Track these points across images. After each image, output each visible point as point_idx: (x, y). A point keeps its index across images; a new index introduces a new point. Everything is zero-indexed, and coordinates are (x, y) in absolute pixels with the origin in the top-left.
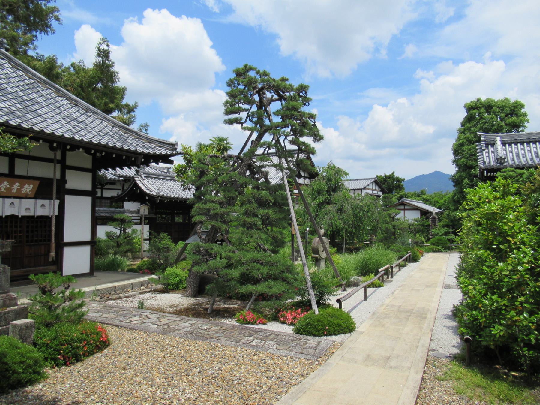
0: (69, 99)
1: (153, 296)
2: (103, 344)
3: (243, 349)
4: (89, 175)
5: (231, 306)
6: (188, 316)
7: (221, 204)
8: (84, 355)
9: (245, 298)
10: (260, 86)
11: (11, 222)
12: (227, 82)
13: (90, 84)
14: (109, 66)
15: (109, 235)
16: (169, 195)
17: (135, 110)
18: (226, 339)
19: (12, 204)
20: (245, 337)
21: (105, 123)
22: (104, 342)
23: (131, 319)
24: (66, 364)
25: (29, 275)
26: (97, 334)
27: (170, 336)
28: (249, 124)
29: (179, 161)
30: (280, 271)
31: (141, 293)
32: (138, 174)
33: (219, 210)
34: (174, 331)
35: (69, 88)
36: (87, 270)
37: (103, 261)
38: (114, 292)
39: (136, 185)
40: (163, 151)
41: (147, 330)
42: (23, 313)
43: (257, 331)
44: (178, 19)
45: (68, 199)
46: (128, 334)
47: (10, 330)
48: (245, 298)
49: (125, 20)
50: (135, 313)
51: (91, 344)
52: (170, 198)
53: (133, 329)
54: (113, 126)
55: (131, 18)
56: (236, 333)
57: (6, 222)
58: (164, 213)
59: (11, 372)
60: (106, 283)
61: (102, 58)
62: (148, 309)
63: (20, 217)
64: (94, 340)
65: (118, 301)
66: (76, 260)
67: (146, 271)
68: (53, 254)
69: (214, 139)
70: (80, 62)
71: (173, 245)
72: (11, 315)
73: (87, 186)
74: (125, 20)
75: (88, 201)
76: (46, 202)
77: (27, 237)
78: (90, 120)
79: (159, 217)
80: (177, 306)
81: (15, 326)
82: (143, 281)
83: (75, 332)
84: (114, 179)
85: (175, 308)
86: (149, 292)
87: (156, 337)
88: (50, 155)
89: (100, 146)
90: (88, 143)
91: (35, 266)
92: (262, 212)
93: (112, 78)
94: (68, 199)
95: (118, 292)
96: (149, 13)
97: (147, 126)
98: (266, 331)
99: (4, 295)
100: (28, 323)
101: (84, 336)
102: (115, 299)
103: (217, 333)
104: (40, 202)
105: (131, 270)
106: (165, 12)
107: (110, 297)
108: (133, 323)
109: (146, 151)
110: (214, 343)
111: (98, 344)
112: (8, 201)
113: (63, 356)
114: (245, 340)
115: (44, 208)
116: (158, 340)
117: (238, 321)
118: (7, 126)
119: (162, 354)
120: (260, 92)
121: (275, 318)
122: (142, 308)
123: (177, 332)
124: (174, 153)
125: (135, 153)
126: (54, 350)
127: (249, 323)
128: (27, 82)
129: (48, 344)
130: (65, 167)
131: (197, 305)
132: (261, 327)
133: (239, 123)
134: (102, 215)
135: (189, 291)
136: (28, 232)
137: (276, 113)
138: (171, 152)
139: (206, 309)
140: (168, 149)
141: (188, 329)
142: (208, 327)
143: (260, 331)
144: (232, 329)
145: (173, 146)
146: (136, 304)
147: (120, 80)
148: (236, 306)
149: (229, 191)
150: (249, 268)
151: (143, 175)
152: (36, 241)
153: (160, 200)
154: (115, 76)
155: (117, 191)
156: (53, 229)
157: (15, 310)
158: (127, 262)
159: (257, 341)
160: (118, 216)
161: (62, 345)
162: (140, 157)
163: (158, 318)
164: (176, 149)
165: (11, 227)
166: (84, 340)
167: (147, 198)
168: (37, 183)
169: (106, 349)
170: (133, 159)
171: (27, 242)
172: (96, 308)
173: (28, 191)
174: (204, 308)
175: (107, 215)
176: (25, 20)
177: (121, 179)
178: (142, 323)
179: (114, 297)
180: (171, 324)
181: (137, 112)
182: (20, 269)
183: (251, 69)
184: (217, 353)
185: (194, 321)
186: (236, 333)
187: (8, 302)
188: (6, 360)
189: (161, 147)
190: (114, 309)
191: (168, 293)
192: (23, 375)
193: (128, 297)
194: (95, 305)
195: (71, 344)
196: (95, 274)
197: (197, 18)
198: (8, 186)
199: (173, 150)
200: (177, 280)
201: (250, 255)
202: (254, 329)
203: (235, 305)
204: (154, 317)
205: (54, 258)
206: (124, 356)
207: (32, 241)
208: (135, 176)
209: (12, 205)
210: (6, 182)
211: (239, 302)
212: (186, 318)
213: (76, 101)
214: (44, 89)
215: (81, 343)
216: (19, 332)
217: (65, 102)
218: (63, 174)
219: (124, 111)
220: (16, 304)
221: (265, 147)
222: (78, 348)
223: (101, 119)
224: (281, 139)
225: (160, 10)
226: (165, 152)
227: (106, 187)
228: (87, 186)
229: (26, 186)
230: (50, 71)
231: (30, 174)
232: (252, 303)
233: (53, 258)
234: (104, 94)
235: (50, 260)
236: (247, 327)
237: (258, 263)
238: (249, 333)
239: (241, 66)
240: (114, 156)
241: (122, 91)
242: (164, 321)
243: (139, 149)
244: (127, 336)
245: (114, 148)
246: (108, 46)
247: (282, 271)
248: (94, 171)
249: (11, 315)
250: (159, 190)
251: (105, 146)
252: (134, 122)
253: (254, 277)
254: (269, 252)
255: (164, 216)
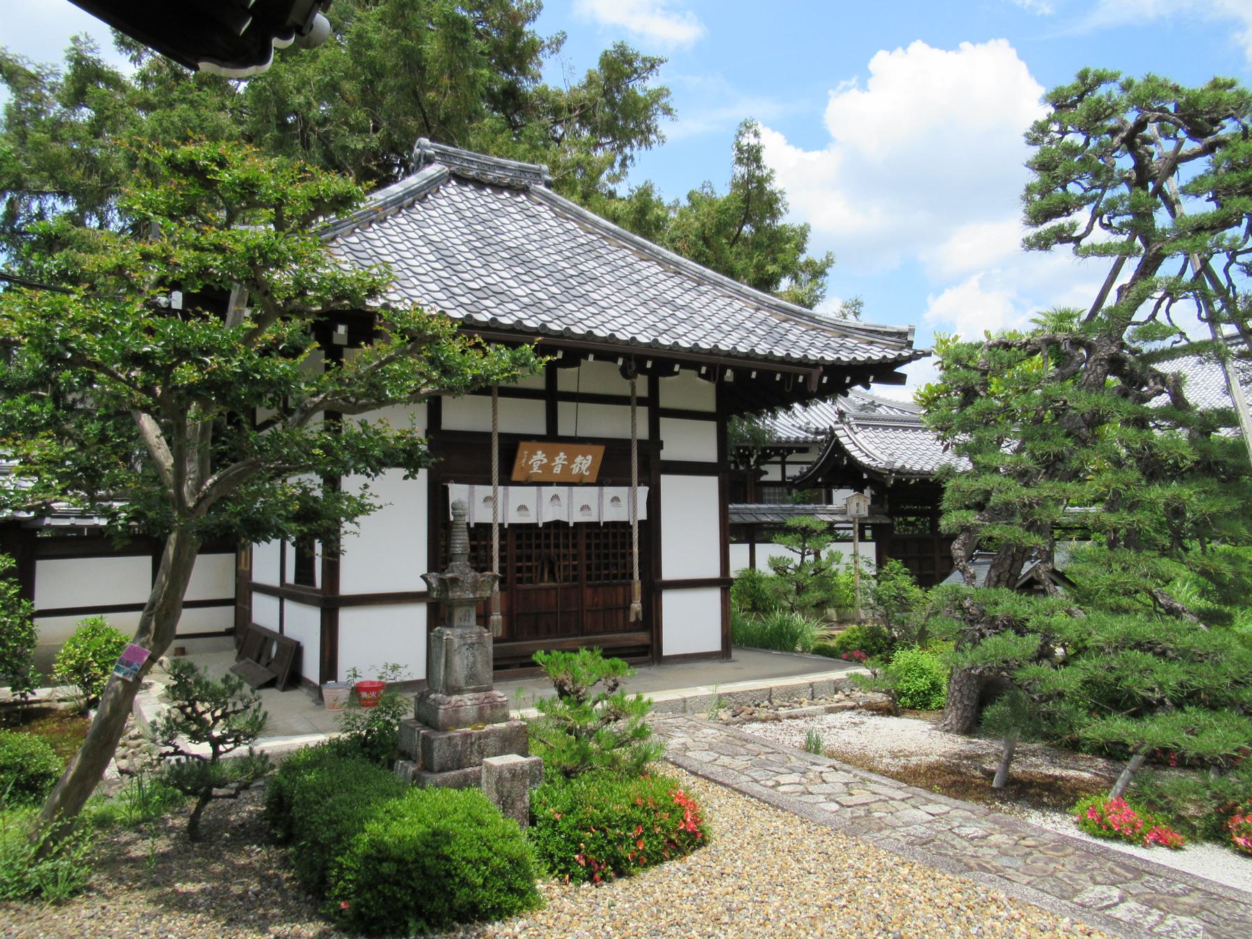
0: (664, 262)
1: (857, 720)
2: (689, 839)
3: (1078, 927)
4: (711, 427)
5: (1071, 773)
6: (929, 788)
7: (1023, 476)
8: (638, 862)
9: (1115, 752)
10: (1131, 117)
11: (557, 537)
12: (1027, 135)
13: (721, 228)
14: (761, 182)
15: (779, 567)
16: (917, 468)
17: (828, 270)
18: (1027, 879)
19: (555, 497)
20: (1096, 883)
21: (737, 305)
22: (688, 834)
23: (779, 778)
24: (591, 878)
25: (535, 652)
26: (673, 811)
27: (865, 842)
28: (1100, 236)
29: (923, 375)
30: (1228, 681)
31: (831, 711)
32: (842, 421)
33: (1016, 493)
34: (880, 830)
35: (679, 245)
36: (716, 646)
37: (756, 624)
38: (766, 703)
39: (839, 447)
40: (876, 353)
41: (811, 814)
42: (517, 740)
43: (1138, 870)
44: (951, 53)
45: (668, 482)
46: (762, 820)
47: (484, 776)
48: (1115, 752)
49: (831, 92)
50: (795, 762)
51: (656, 836)
52: (920, 473)
53: (778, 807)
54: (757, 309)
55: (843, 83)
56: (1066, 867)
57: (547, 536)
58: (911, 513)
59: (457, 880)
60: (752, 678)
61: (747, 165)
62: (831, 755)
63: (571, 525)
64: (663, 826)
65: (768, 725)
66: (690, 621)
67: (857, 654)
68: (637, 606)
69: (1042, 318)
70: (704, 187)
71: (917, 592)
72: (492, 741)
73: (709, 453)
74: (831, 92)
75: (709, 486)
76: (622, 492)
77: (589, 567)
78: (704, 300)
79: (900, 524)
80: (912, 754)
81: (490, 768)
82: (841, 680)
83: (618, 799)
84: (805, 441)
85: (903, 761)
86: (852, 708)
87: (827, 839)
88: (621, 387)
89: (717, 355)
90: (690, 350)
91: (606, 631)
92: (1159, 493)
93: (771, 206)
94: (668, 482)
95: (777, 702)
96: (881, 62)
97: (858, 304)
98: (1172, 875)
99: (482, 695)
100: (515, 764)
101: (637, 814)
102: (764, 721)
103: (1004, 854)
104: (610, 491)
105: (822, 651)
106: (918, 48)
107: (756, 715)
108: (781, 789)
109: (830, 356)
110: (985, 886)
111: (673, 837)
112: (548, 491)
113: (585, 858)
114: (1092, 893)
115: (618, 505)
116: (830, 851)
117: (1082, 824)
118: (545, 335)
119: (825, 895)
120: (1133, 140)
121: (1217, 833)
122: (817, 752)
123: (886, 833)
124: (905, 353)
125: (804, 363)
126: (567, 840)
127: (1117, 838)
128: (582, 240)
129: (556, 821)
130: (657, 413)
131: (967, 758)
132: (1160, 856)
133: (1069, 239)
134: (764, 519)
135: (952, 717)
136: (589, 557)
137: (1193, 189)
138: (896, 353)
139: (990, 774)
140: (888, 346)
141: (920, 830)
142: (981, 833)
143: (1154, 871)
144: (1054, 849)
145: (902, 338)
146: (800, 739)
147: (789, 208)
148: (1086, 775)
149: (1045, 437)
150: (1114, 664)
151: (853, 423)
152: (607, 576)
153: (897, 481)
154: (777, 200)
155: (799, 466)
156: (636, 550)
157: (500, 731)
158: (815, 631)
159: (1132, 904)
160: (792, 522)
161: (586, 829)
162: (816, 373)
163: (846, 784)
164: (910, 344)
165: (557, 546)
166: (639, 823)
167: (865, 476)
168: (601, 450)
169: (695, 853)
170: (801, 379)
171: (589, 578)
172: (709, 739)
173: (584, 468)
174: (984, 771)
175: (777, 519)
176: (609, 129)
177: (819, 437)
178: (803, 793)
179: (763, 715)
180: (874, 806)
181: (832, 279)
182: (576, 635)
183: (1100, 80)
184: (989, 922)
185: (942, 805)
186: (1066, 867)
187: (489, 711)
188: (447, 850)
189: (871, 343)
190: (750, 746)
191: (897, 715)
192: (482, 893)
193: (796, 717)
194: (710, 731)
195: (603, 830)
196: (735, 654)
197: (996, 38)
198: (545, 461)
199: (902, 349)
200: (922, 684)
201: (1119, 626)
202: (1131, 863)
203: (1082, 772)
204: (837, 779)
205: (640, 616)
206: (730, 880)
207: (598, 578)
208: (835, 426)
209: (556, 502)
210: (539, 453)
211: (1101, 763)
212: (923, 793)
213: (677, 264)
214: (613, 248)
215: (629, 829)
216: (496, 783)
217: (656, 269)
218: (654, 428)
219: (804, 277)
220: (506, 718)
221: (1158, 295)
222: (621, 840)
223: (730, 297)
224: (1218, 263)
225: (905, 48)
226: (881, 355)
227: (789, 459)
228: (709, 453)
229: (579, 459)
230: (643, 219)
231: (582, 433)
232: (1133, 772)
233: (637, 614)
234: (757, 245)
235: (633, 619)
236: (1107, 850)
237: (1150, 649)
238: (1111, 870)
239: (1068, 80)
240: (754, 375)
241: (802, 234)
242: (861, 796)
243: (814, 354)
244: (757, 824)
245: (751, 356)
246: (756, 134)
247: (1236, 682)
248: (721, 416)
249: (492, 741)
250: (891, 455)
251: (728, 354)
252: (823, 297)
253: (1131, 697)
254: (1189, 619)
255: (911, 519)
